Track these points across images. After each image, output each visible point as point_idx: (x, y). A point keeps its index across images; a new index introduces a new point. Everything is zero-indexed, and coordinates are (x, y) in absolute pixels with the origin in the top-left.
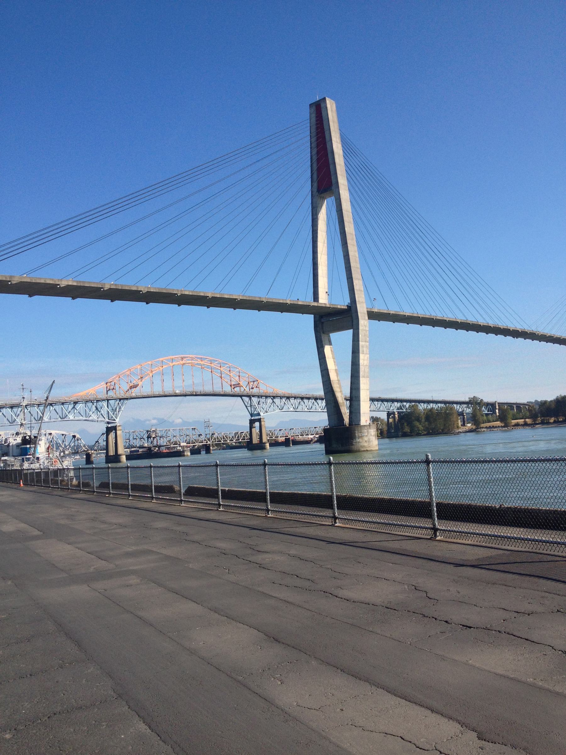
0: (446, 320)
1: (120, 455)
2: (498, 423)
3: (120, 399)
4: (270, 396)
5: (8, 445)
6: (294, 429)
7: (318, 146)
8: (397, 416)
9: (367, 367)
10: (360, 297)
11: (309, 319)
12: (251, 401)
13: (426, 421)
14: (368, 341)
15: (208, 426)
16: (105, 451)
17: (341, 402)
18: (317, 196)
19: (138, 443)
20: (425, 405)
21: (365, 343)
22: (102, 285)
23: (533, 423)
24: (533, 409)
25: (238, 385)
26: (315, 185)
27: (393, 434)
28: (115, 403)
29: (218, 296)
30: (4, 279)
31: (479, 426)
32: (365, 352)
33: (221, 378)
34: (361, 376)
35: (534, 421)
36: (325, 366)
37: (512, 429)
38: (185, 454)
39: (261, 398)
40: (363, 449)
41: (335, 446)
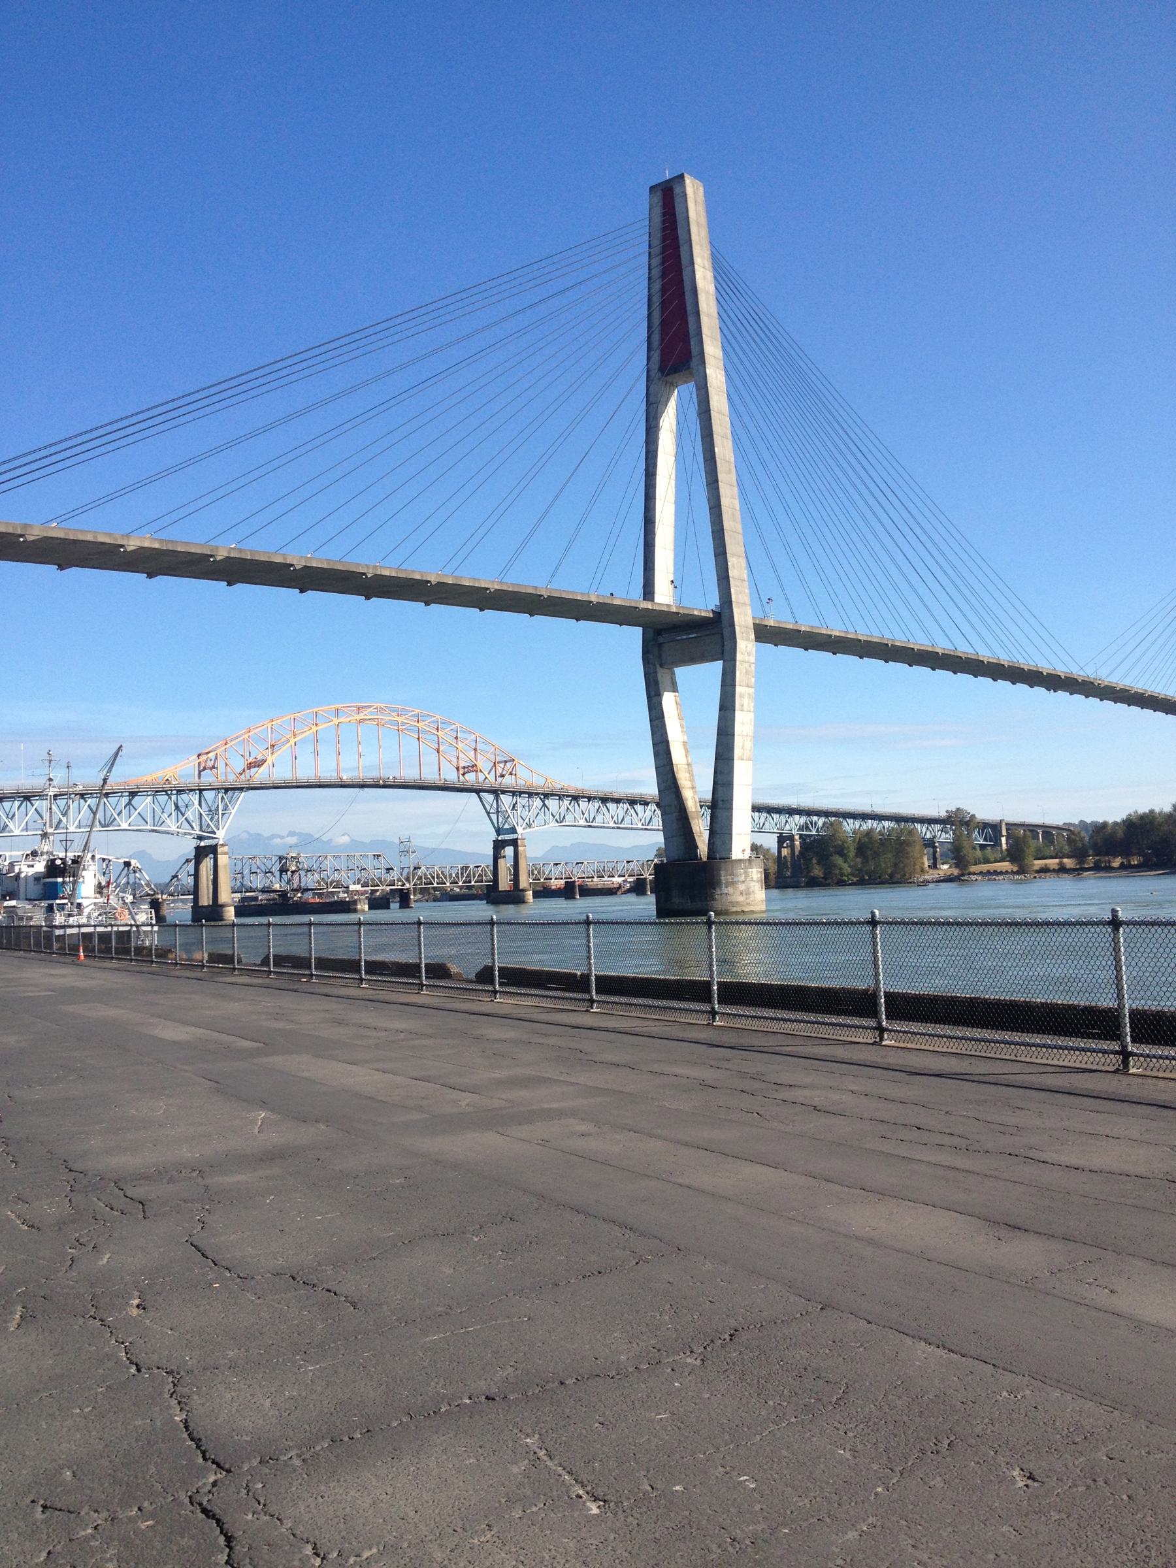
0: (913, 649)
1: (223, 906)
2: (1006, 865)
3: (227, 790)
4: (537, 794)
5: (17, 877)
6: (586, 863)
7: (664, 274)
8: (797, 843)
9: (749, 738)
10: (740, 593)
11: (635, 634)
12: (497, 802)
13: (857, 856)
14: (753, 685)
15: (408, 852)
16: (192, 897)
17: (694, 810)
18: (659, 379)
19: (258, 882)
20: (857, 823)
22: (211, 550)
23: (1078, 867)
25: (473, 768)
26: (656, 356)
27: (788, 880)
28: (215, 798)
30: (11, 530)
31: (965, 870)
32: (746, 708)
33: (438, 752)
35: (1081, 862)
36: (662, 735)
37: (1035, 877)
38: (359, 907)
39: (520, 796)
40: (734, 909)
41: (677, 901)
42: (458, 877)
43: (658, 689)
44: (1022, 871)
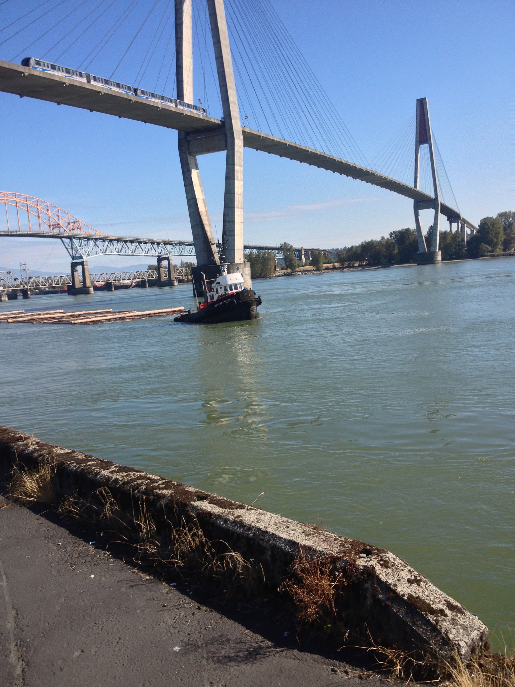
2: (311, 267)
4: (92, 239)
9: (241, 196)
12: (71, 243)
15: (25, 270)
21: (239, 167)
24: (341, 254)
29: (78, 85)
34: (236, 206)
35: (342, 264)
36: (192, 194)
38: (3, 299)
42: (52, 282)
43: (189, 168)
44: (318, 270)
